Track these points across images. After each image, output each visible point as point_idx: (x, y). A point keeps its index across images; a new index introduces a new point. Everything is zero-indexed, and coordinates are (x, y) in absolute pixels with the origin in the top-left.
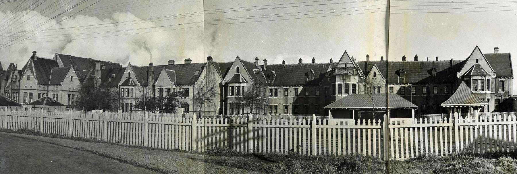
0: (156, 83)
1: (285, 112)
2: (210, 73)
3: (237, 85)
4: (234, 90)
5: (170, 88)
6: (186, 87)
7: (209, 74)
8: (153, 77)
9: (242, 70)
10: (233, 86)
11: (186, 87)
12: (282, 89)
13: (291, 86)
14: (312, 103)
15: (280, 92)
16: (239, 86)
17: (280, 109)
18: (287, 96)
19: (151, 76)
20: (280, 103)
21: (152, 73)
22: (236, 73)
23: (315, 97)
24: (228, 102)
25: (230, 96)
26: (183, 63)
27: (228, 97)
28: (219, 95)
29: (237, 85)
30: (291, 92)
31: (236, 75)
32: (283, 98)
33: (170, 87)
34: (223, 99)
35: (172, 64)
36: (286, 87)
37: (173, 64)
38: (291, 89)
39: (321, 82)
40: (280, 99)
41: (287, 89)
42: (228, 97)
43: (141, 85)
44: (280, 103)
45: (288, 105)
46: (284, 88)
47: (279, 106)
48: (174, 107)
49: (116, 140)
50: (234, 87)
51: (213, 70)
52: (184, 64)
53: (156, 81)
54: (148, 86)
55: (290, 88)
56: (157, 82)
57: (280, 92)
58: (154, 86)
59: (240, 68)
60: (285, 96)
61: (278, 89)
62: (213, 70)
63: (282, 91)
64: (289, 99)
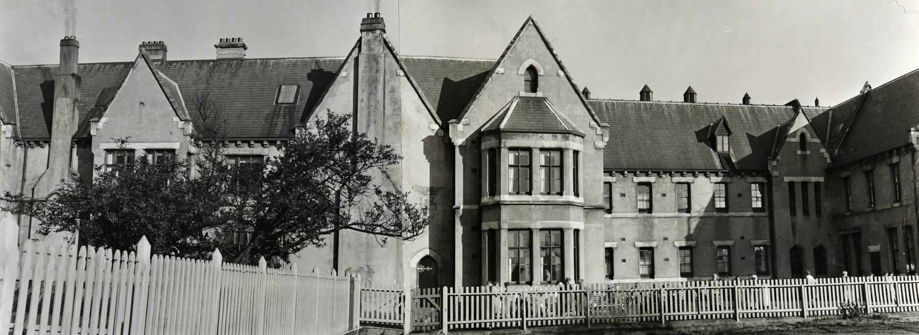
0: (100, 125)
1: (641, 272)
2: (376, 88)
3: (549, 141)
4: (504, 167)
5: (172, 151)
6: (245, 150)
7: (370, 94)
8: (76, 100)
9: (553, 80)
10: (529, 150)
11: (245, 150)
12: (630, 184)
13: (665, 173)
14: (743, 238)
15: (623, 195)
16: (561, 150)
17: (624, 261)
18: (650, 210)
19: (66, 94)
20: (623, 239)
21: (74, 82)
22: (523, 94)
23: (752, 216)
24: (505, 226)
25: (510, 194)
26: (212, 55)
27: (505, 197)
28: (423, 193)
29: (549, 141)
30: (664, 195)
31: (526, 100)
32: (637, 218)
33: (176, 146)
34: (461, 212)
35: (158, 60)
36: (647, 175)
37: (160, 57)
38: (664, 186)
39: (775, 163)
40: (623, 221)
41: (649, 184)
42: (505, 197)
43: (16, 138)
44: (623, 239)
45: (654, 244)
46: (636, 180)
47: (619, 250)
48: (186, 244)
49: (71, 83)
50: (536, 152)
51: (387, 77)
52: (216, 59)
53: (100, 116)
54: (48, 141)
55: (661, 180)
56: (103, 120)
57: (623, 195)
58: (83, 141)
59: (541, 73)
60: (641, 211)
61: (614, 185)
62: (392, 76)
63: (631, 189)
64: (656, 221)
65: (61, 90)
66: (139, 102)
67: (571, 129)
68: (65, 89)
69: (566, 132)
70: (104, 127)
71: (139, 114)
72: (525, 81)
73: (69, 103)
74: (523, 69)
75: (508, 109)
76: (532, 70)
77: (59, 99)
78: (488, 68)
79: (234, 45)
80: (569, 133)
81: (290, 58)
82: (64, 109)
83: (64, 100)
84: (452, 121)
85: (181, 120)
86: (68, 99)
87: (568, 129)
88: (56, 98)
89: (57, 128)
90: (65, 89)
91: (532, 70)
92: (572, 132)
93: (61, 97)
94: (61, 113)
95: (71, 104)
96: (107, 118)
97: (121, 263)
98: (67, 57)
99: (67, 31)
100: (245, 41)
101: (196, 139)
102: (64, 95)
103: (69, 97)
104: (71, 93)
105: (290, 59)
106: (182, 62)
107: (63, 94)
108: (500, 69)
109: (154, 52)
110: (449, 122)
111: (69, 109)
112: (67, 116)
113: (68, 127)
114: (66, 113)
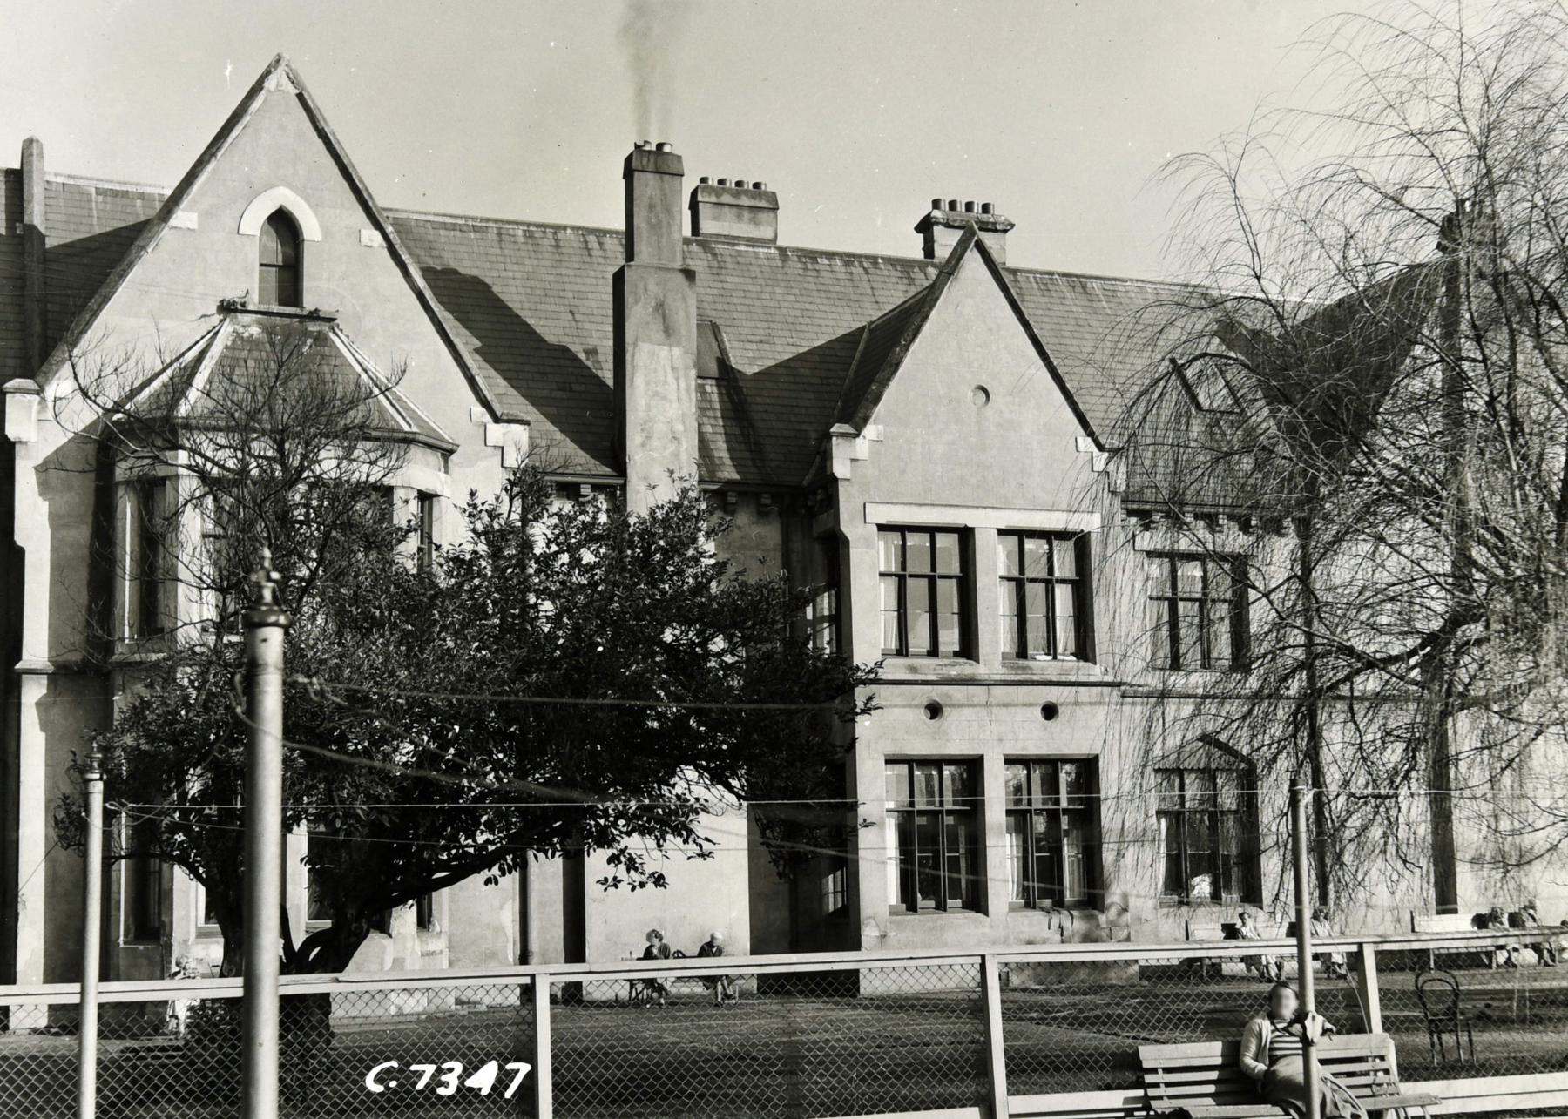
56: (870, 431)
65: (649, 319)
66: (973, 387)
67: (414, 429)
68: (664, 317)
69: (400, 435)
70: (874, 453)
71: (978, 422)
72: (262, 265)
73: (678, 363)
74: (255, 219)
75: (202, 354)
76: (283, 223)
77: (645, 347)
78: (141, 213)
79: (988, 223)
80: (408, 440)
81: (1143, 281)
82: (666, 382)
83: (664, 351)
84: (16, 382)
85: (497, 420)
86: (676, 351)
87: (406, 428)
88: (635, 345)
89: (643, 445)
90: (664, 317)
91: (283, 223)
92: (420, 438)
93: (650, 341)
94: (656, 394)
95: (686, 368)
96: (881, 427)
97: (665, 953)
98: (659, 208)
99: (643, 117)
100: (1000, 213)
101: (319, 477)
102: (660, 336)
103: (678, 344)
104: (683, 332)
105: (1139, 284)
106: (849, 259)
107: (657, 327)
108: (183, 217)
109: (746, 215)
110: (8, 385)
111: (683, 385)
112: (675, 405)
113: (684, 445)
114: (674, 397)
